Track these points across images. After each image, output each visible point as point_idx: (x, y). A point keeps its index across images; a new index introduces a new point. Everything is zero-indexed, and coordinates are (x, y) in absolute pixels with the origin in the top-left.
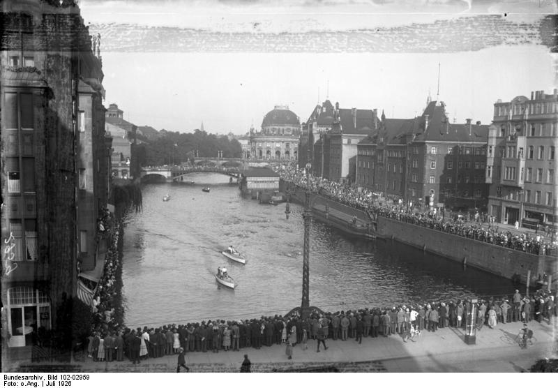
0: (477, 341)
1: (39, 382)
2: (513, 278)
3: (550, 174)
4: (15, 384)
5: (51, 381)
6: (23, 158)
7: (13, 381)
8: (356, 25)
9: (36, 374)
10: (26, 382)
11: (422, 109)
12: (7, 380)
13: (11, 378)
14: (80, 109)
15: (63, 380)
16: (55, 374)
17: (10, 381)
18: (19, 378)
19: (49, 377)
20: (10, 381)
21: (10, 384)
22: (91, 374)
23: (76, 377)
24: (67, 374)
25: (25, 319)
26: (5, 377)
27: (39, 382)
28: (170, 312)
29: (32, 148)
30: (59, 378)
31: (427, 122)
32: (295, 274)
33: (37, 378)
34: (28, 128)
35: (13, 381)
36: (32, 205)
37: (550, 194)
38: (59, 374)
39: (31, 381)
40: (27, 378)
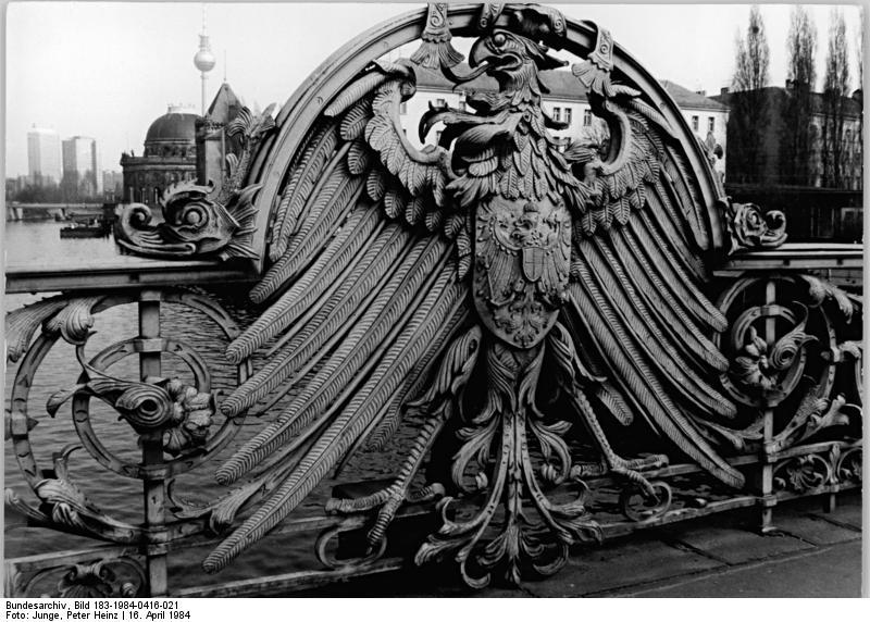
0: (59, 233)
1: (62, 613)
2: (826, 298)
3: (677, 153)
4: (23, 616)
5: (82, 611)
7: (21, 611)
9: (57, 600)
10: (32, 612)
11: (734, 57)
12: (11, 610)
13: (17, 606)
14: (405, 86)
15: (98, 609)
16: (86, 600)
17: (15, 611)
18: (30, 606)
19: (77, 605)
20: (15, 611)
21: (16, 616)
24: (104, 600)
25: (32, 202)
26: (8, 605)
27: (62, 613)
29: (194, 410)
30: (92, 605)
32: (809, 472)
33: (58, 607)
34: (589, 335)
35: (21, 611)
38: (92, 601)
39: (154, 611)
40: (42, 606)
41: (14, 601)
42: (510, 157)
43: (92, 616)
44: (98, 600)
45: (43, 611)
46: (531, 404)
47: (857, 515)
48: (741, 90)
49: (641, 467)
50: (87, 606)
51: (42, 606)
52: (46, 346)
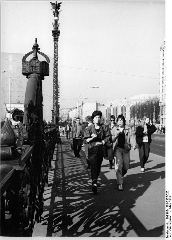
4: (171, 234)
5: (169, 218)
6: (9, 103)
7: (169, 234)
8: (75, 203)
9: (166, 224)
10: (169, 232)
12: (169, 237)
16: (166, 216)
17: (169, 236)
18: (168, 232)
19: (167, 219)
20: (169, 236)
22: (166, 190)
23: (167, 193)
24: (166, 211)
26: (167, 238)
28: (76, 132)
30: (167, 215)
31: (32, 165)
35: (169, 234)
36: (21, 112)
37: (82, 110)
40: (168, 228)
41: (166, 236)
42: (105, 174)
43: (170, 202)
44: (166, 213)
45: (169, 228)
46: (95, 223)
47: (11, 58)
48: (47, 226)
49: (135, 123)
50: (168, 216)
51: (168, 228)
52: (143, 155)
